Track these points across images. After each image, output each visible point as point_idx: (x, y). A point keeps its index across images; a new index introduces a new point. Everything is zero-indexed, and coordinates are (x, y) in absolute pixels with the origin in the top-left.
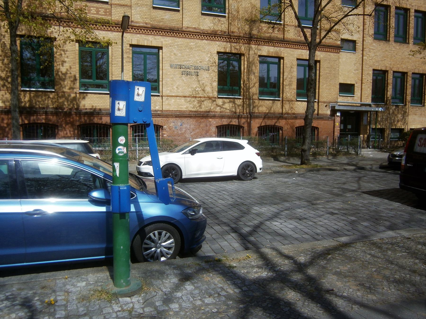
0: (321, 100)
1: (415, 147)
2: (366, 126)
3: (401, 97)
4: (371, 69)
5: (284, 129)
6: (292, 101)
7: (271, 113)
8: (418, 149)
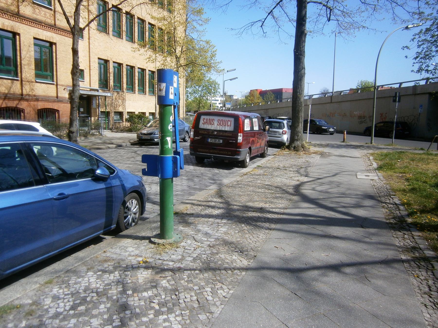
0: (59, 83)
1: (200, 125)
2: (96, 109)
3: (142, 88)
5: (26, 112)
6: (32, 82)
7: (11, 94)
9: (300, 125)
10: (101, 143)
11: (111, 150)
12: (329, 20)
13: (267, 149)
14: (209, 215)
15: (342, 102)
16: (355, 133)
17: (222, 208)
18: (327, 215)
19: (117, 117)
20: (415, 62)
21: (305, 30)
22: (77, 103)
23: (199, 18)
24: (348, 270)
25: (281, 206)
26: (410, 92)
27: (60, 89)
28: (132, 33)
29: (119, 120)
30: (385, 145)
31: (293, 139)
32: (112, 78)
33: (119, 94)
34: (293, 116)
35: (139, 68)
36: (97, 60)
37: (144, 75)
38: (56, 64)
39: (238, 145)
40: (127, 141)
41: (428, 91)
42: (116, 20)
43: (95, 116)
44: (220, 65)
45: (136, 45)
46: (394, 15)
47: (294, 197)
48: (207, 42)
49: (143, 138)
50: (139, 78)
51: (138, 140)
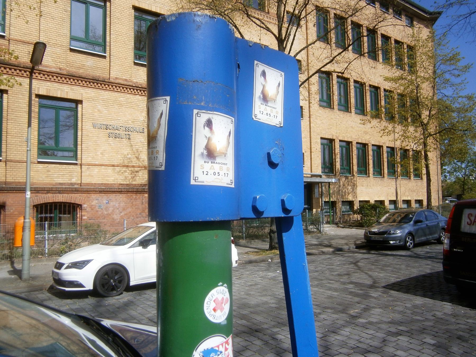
1: (463, 226)
2: (318, 199)
3: (379, 170)
8: (465, 227)
10: (316, 245)
11: (323, 257)
19: (346, 208)
28: (364, 104)
32: (338, 160)
35: (373, 145)
36: (319, 141)
40: (352, 241)
49: (373, 239)
51: (365, 241)
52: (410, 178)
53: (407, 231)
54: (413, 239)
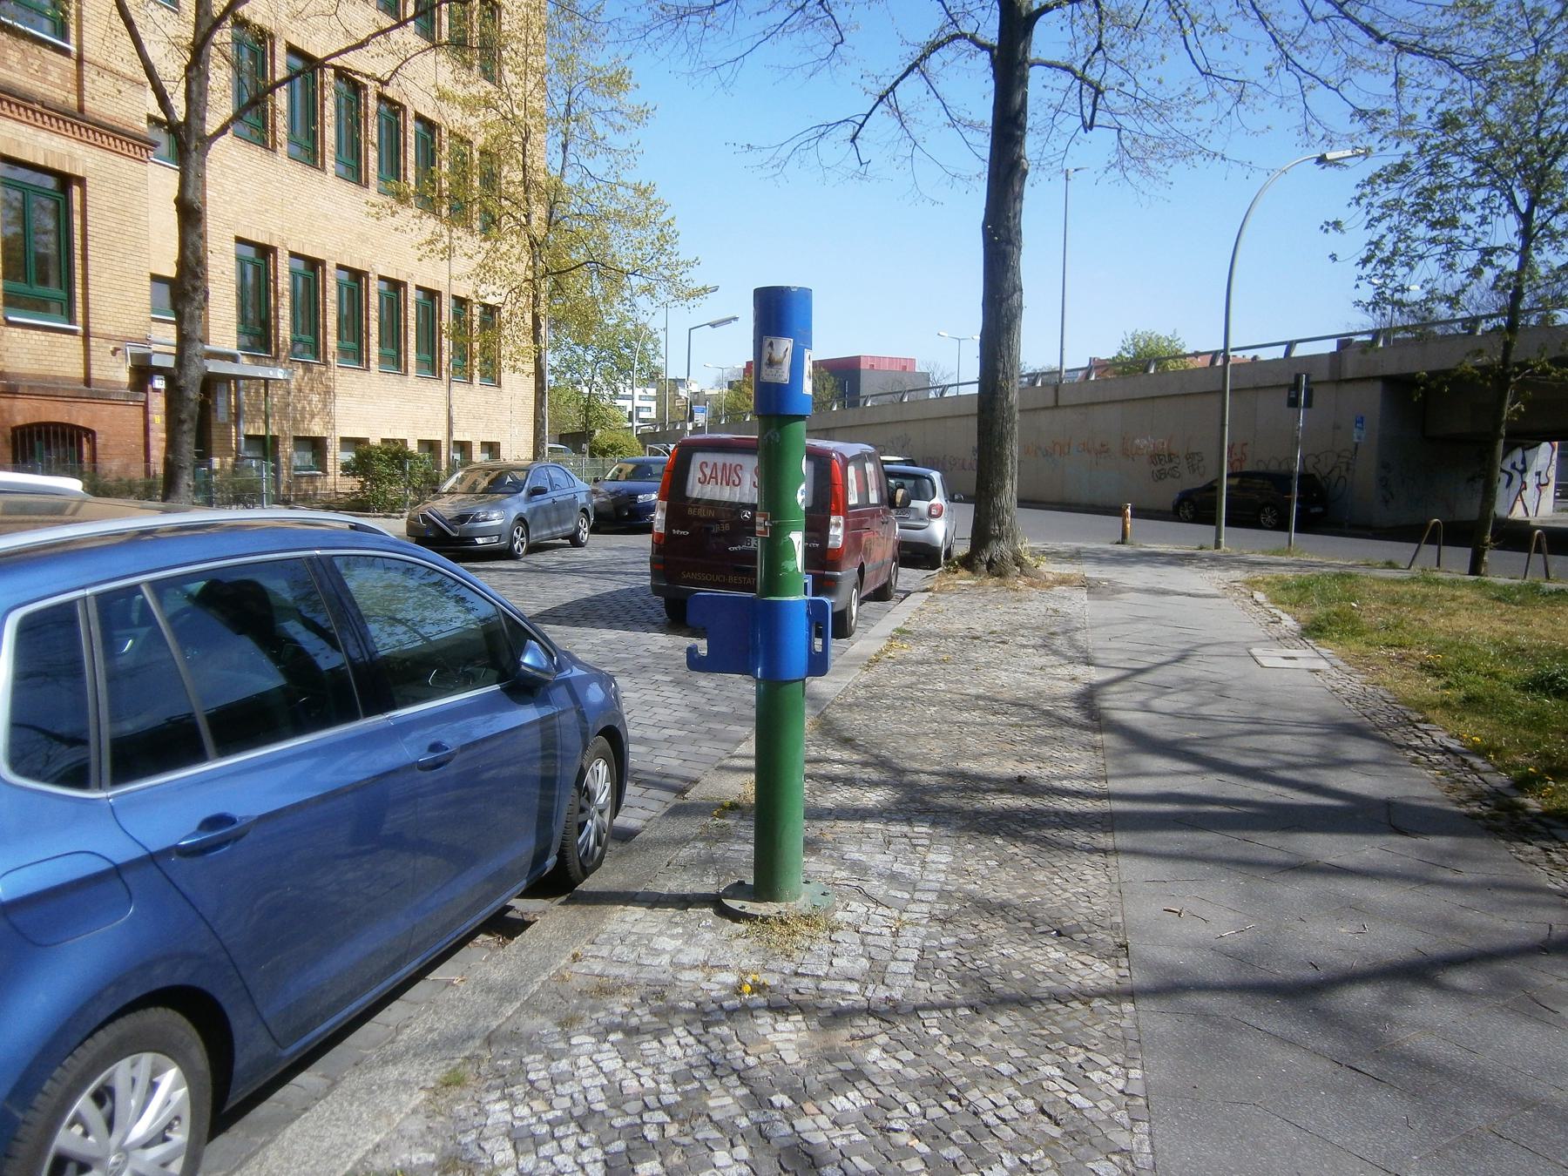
0: (95, 327)
1: (689, 486)
2: (227, 426)
3: (355, 345)
4: (231, 236)
8: (697, 488)
9: (1008, 487)
12: (1089, 126)
13: (896, 569)
14: (856, 811)
15: (1093, 404)
16: (1093, 506)
17: (884, 783)
18: (1258, 797)
20: (1364, 273)
21: (1021, 157)
22: (192, 405)
23: (612, 104)
24: (1461, 979)
25: (1079, 768)
26: (1323, 374)
27: (100, 349)
29: (311, 469)
30: (1263, 552)
31: (982, 535)
32: (285, 312)
33: (310, 370)
34: (1014, 454)
36: (231, 246)
37: (399, 303)
38: (85, 258)
39: (829, 557)
41: (1380, 372)
42: (300, 101)
43: (226, 451)
44: (693, 273)
45: (372, 194)
46: (1309, 118)
47: (1099, 737)
48: (643, 193)
50: (381, 317)
52: (471, 382)
53: (514, 514)
54: (527, 534)
